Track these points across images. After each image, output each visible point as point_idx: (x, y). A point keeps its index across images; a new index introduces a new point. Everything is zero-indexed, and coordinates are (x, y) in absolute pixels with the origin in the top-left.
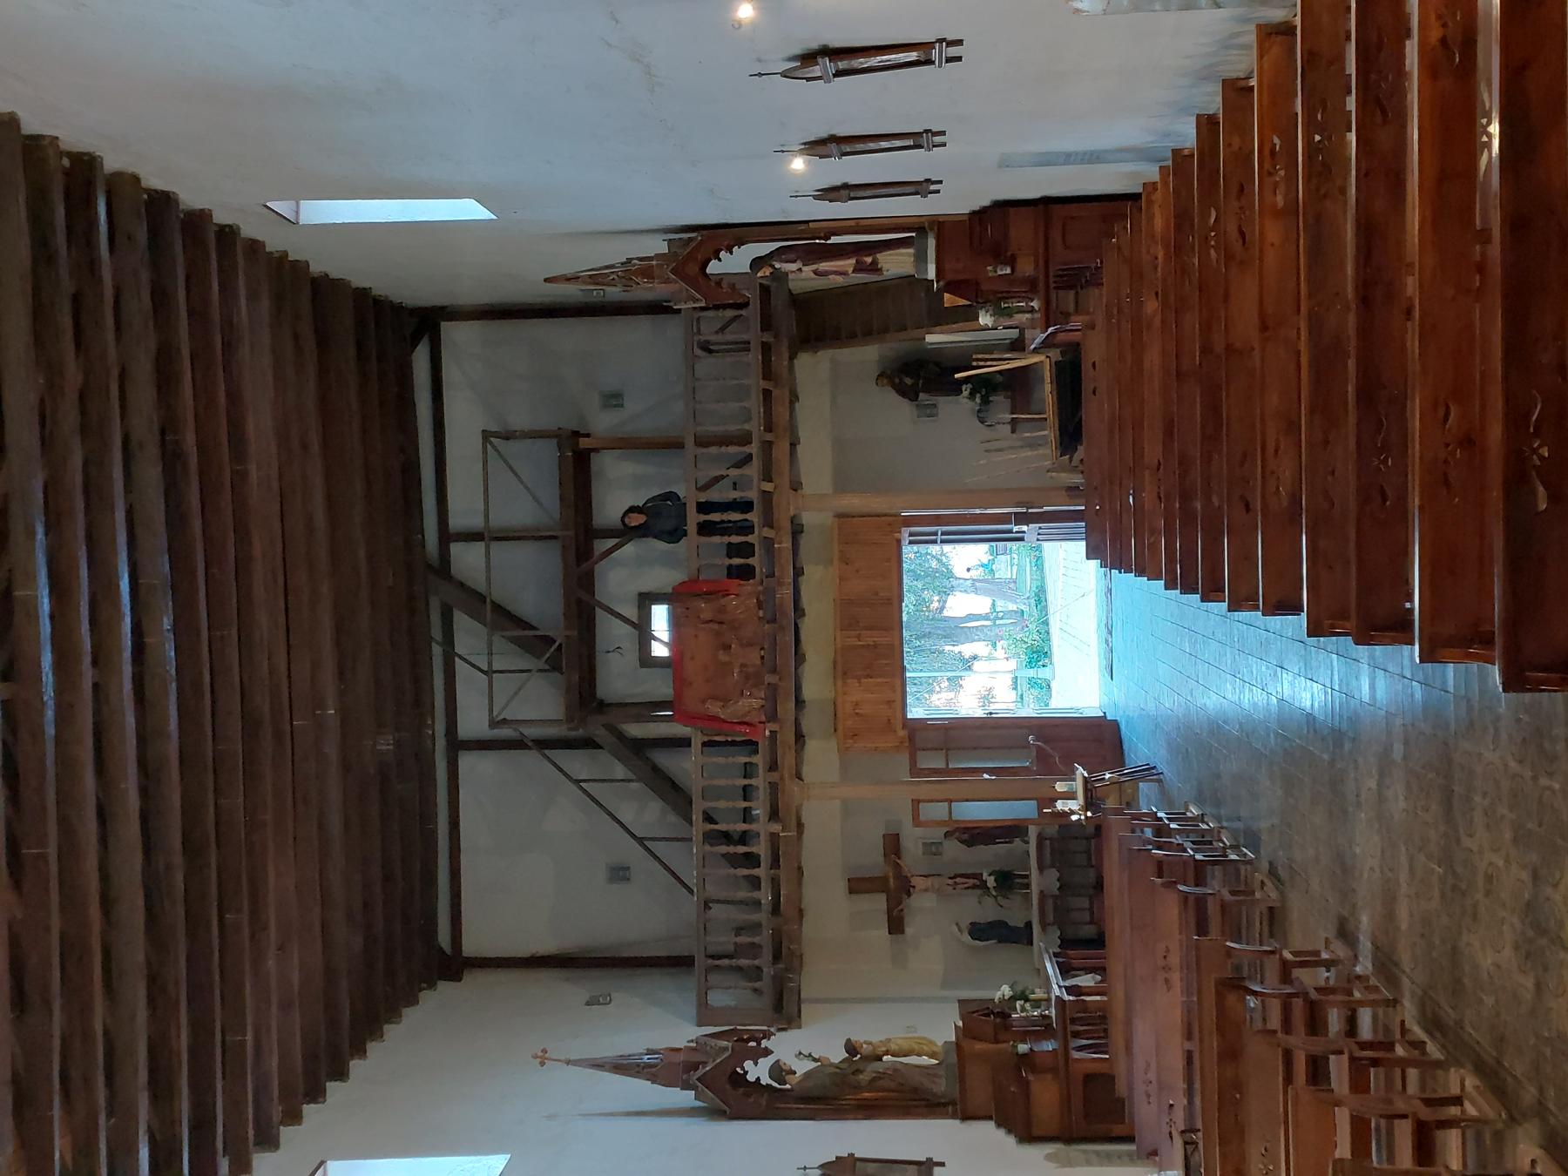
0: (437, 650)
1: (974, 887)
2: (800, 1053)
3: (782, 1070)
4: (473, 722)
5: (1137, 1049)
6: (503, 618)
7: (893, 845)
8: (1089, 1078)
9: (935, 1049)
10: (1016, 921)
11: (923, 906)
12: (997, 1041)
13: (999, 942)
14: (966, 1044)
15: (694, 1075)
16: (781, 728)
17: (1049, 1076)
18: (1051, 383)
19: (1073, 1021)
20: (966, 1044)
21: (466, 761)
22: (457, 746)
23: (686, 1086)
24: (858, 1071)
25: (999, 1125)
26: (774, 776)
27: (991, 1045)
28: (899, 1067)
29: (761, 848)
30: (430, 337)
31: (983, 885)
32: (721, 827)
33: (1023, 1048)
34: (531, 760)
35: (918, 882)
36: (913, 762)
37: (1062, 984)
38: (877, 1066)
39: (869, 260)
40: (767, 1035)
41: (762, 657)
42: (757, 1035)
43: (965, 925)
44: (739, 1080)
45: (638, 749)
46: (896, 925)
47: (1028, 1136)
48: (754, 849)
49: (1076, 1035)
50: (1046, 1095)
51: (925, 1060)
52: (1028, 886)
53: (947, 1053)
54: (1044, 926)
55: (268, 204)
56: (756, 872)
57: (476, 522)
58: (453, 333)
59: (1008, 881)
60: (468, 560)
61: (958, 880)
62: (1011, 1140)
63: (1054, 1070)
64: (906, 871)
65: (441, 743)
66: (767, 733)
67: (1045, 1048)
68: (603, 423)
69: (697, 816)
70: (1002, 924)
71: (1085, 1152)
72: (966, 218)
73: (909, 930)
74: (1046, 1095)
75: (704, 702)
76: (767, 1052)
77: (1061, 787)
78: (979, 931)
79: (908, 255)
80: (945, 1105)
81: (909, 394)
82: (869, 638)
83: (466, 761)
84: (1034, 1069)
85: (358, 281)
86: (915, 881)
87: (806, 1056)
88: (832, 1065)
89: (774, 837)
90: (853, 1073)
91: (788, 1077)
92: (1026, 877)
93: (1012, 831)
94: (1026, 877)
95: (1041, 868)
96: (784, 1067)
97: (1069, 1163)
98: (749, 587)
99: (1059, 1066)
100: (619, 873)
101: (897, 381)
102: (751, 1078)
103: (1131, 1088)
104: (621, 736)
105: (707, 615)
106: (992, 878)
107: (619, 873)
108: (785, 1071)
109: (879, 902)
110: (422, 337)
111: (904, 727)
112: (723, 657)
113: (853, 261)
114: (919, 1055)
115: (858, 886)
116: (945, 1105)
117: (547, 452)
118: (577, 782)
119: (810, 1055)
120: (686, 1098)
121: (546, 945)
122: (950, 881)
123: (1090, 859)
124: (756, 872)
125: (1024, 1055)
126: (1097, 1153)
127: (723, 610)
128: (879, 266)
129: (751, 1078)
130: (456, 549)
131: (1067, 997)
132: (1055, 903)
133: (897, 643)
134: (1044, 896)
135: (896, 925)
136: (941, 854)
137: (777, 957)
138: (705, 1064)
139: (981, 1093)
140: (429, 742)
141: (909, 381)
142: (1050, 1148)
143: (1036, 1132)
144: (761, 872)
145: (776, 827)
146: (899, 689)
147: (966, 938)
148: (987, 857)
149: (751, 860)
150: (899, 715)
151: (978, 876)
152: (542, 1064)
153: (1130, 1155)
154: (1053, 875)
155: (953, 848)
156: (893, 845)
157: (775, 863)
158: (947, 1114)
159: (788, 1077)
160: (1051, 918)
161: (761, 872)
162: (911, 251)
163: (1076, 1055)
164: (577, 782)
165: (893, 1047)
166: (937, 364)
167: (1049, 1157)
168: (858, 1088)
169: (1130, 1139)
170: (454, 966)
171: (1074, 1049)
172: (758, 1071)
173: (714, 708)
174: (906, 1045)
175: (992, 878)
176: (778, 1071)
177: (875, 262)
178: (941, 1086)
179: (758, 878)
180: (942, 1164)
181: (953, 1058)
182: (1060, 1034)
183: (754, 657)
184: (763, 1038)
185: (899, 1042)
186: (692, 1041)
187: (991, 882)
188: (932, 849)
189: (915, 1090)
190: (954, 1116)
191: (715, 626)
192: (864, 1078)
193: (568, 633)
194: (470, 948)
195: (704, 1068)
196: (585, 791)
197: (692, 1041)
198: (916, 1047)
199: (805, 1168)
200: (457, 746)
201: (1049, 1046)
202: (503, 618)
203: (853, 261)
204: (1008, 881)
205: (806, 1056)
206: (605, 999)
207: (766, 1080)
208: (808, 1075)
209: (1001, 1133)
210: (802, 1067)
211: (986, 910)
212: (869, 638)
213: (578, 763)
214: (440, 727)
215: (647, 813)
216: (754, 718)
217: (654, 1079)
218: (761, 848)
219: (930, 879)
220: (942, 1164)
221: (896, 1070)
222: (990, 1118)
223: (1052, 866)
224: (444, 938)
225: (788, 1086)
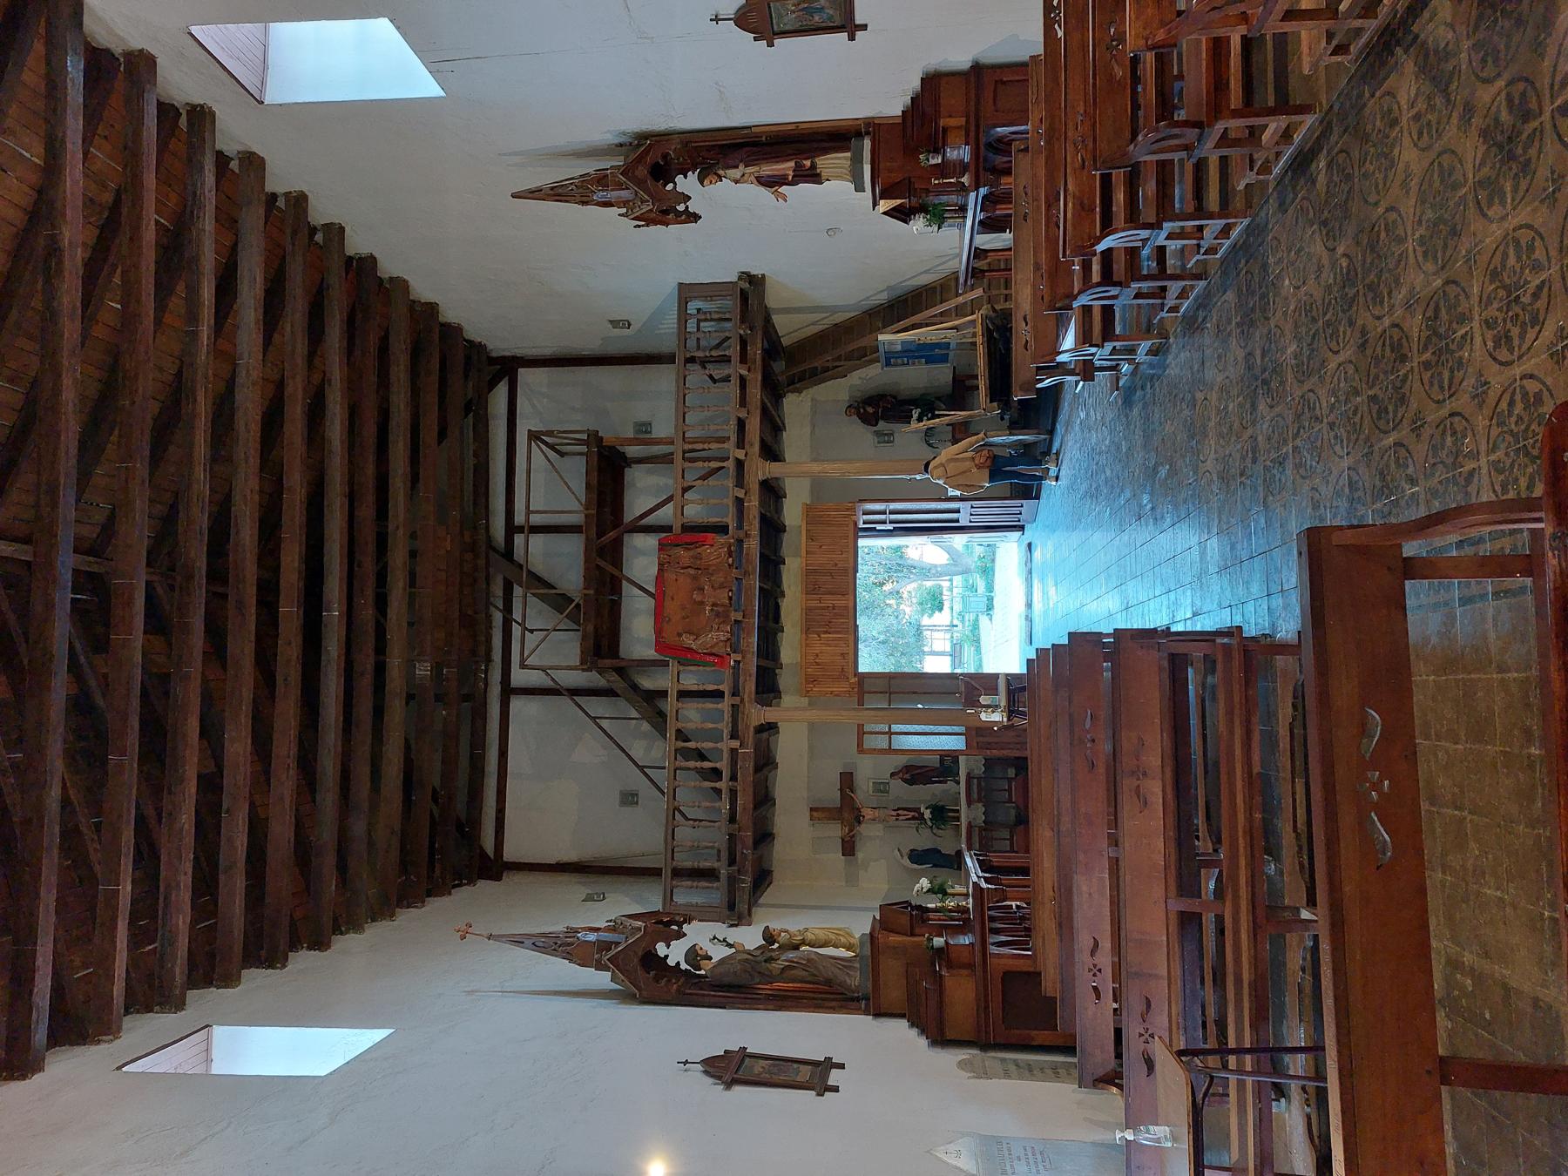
0: (498, 618)
1: (913, 818)
2: (715, 938)
3: (698, 955)
5: (1079, 921)
7: (847, 780)
8: (1009, 977)
9: (852, 941)
10: (948, 849)
11: (872, 833)
12: (912, 935)
13: (935, 866)
14: (881, 937)
15: (606, 955)
16: (743, 657)
17: (965, 972)
18: (983, 335)
19: (990, 909)
20: (881, 937)
21: (516, 704)
23: (600, 967)
24: (770, 960)
25: (913, 1025)
26: (737, 700)
27: (905, 938)
28: (813, 956)
29: (723, 765)
30: (509, 380)
31: (921, 817)
32: (692, 745)
33: (938, 941)
34: (565, 701)
37: (980, 875)
38: (791, 955)
39: (808, 163)
41: (730, 598)
42: (677, 918)
43: (906, 851)
44: (654, 963)
46: (849, 848)
47: (940, 1038)
48: (718, 765)
49: (997, 932)
50: (961, 991)
51: (842, 953)
52: (958, 819)
53: (862, 944)
54: (969, 849)
55: (195, 30)
56: (717, 785)
58: (524, 374)
59: (942, 814)
61: (900, 812)
62: (923, 1042)
63: (970, 966)
65: (495, 691)
66: (732, 663)
67: (962, 942)
69: (671, 734)
70: (936, 851)
71: (1003, 1060)
72: (900, 121)
73: (860, 855)
74: (961, 991)
75: (680, 635)
77: (985, 700)
78: (917, 857)
79: (845, 158)
80: (858, 999)
81: (869, 420)
82: (829, 601)
83: (516, 704)
84: (950, 965)
85: (423, 290)
86: (865, 812)
87: (720, 941)
88: (749, 953)
89: (733, 751)
90: (765, 961)
91: (703, 963)
92: (958, 811)
93: (946, 765)
94: (958, 811)
95: (969, 803)
96: (700, 952)
97: (985, 1074)
98: (721, 539)
99: (977, 962)
100: (630, 798)
101: (862, 411)
102: (671, 962)
103: (1067, 981)
104: (635, 687)
105: (686, 561)
106: (928, 811)
107: (630, 798)
108: (700, 956)
109: (835, 831)
110: (501, 381)
111: (855, 675)
112: (697, 596)
113: (792, 164)
114: (836, 946)
115: (819, 813)
116: (858, 999)
118: (594, 719)
119: (725, 940)
120: (603, 979)
121: (571, 856)
122: (894, 813)
123: (1010, 795)
124: (717, 785)
125: (940, 950)
126: (1016, 1063)
127: (698, 557)
128: (818, 171)
129: (671, 962)
130: (519, 539)
131: (984, 885)
132: (979, 784)
133: (851, 604)
134: (971, 827)
135: (849, 848)
136: (888, 792)
138: (617, 944)
139: (894, 992)
140: (481, 684)
141: (870, 410)
143: (949, 1035)
145: (735, 744)
146: (852, 644)
147: (907, 862)
148: (924, 794)
149: (716, 774)
150: (851, 670)
151: (917, 810)
152: (463, 938)
153: (1055, 1067)
154: (979, 809)
155: (898, 788)
156: (847, 780)
157: (733, 778)
158: (860, 1009)
159: (703, 963)
160: (975, 796)
161: (723, 785)
162: (848, 154)
163: (994, 950)
164: (594, 719)
165: (810, 936)
166: (895, 397)
167: (962, 1065)
168: (770, 978)
169: (1069, 1050)
170: (493, 867)
171: (993, 944)
172: (674, 953)
173: (688, 641)
174: (822, 935)
175: (928, 811)
176: (694, 955)
177: (813, 166)
178: (854, 980)
179: (721, 790)
180: (842, 1066)
181: (867, 951)
182: (978, 927)
183: (723, 597)
184: (685, 922)
185: (817, 931)
186: (611, 921)
187: (927, 814)
188: (882, 788)
189: (828, 982)
190: (867, 1013)
191: (692, 572)
192: (776, 966)
193: (587, 592)
194: (510, 854)
195: (615, 948)
196: (600, 728)
197: (611, 921)
198: (833, 937)
199: (686, 1062)
201: (966, 940)
203: (792, 164)
204: (942, 814)
205: (720, 941)
206: (599, 895)
208: (722, 961)
209: (914, 1032)
210: (718, 953)
211: (923, 839)
212: (829, 601)
213: (597, 706)
214: (496, 675)
215: (651, 749)
216: (720, 650)
217: (569, 957)
218: (723, 765)
219: (877, 811)
220: (842, 1066)
221: (810, 961)
222: (902, 1016)
223: (979, 800)
224: (488, 844)
225: (703, 972)
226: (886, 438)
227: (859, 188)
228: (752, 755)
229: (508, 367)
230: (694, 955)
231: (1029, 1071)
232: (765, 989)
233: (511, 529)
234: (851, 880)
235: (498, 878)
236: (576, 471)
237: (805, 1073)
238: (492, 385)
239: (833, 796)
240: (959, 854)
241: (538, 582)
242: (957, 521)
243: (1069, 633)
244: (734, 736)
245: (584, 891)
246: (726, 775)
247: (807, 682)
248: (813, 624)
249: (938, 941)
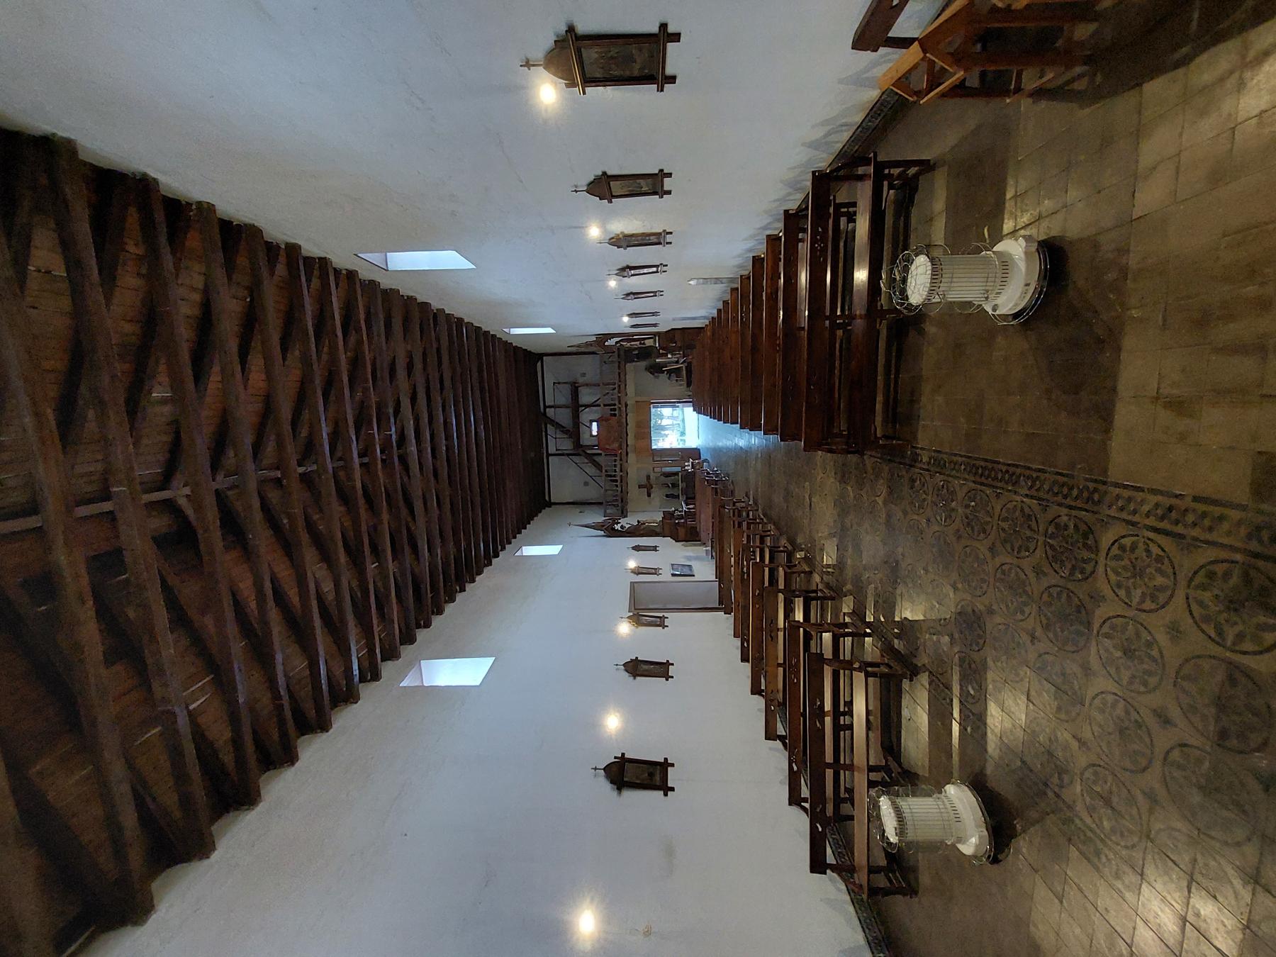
0: (544, 433)
4: (552, 450)
6: (558, 426)
7: (648, 477)
10: (676, 494)
21: (550, 458)
22: (548, 455)
29: (618, 478)
31: (669, 486)
35: (654, 486)
36: (653, 459)
40: (620, 519)
45: (591, 458)
46: (649, 495)
50: (682, 532)
57: (552, 404)
59: (674, 485)
60: (550, 412)
64: (652, 483)
68: (581, 380)
69: (604, 471)
76: (620, 523)
93: (676, 474)
95: (682, 482)
100: (586, 484)
104: (586, 453)
117: (568, 387)
120: (602, 533)
130: (547, 410)
135: (649, 495)
137: (622, 501)
139: (667, 531)
142: (682, 543)
144: (618, 483)
145: (621, 474)
148: (669, 480)
149: (616, 481)
154: (684, 484)
156: (648, 477)
157: (621, 482)
161: (618, 483)
167: (682, 545)
172: (618, 527)
176: (622, 527)
178: (658, 530)
187: (670, 485)
200: (548, 455)
201: (682, 521)
202: (558, 426)
207: (620, 529)
210: (627, 526)
215: (591, 470)
218: (618, 478)
224: (547, 498)
226: (657, 377)
227: (808, 816)
228: (838, 623)
229: (540, 356)
230: (622, 527)
231: (695, 545)
232: (637, 533)
233: (545, 407)
234: (650, 503)
235: (550, 507)
236: (566, 389)
237: (652, 549)
238: (538, 362)
239: (644, 481)
240: (679, 495)
241: (553, 422)
242: (655, 325)
243: (752, 694)
244: (621, 471)
245: (579, 510)
246: (619, 481)
247: (695, 514)
248: (637, 437)
249: (677, 521)
